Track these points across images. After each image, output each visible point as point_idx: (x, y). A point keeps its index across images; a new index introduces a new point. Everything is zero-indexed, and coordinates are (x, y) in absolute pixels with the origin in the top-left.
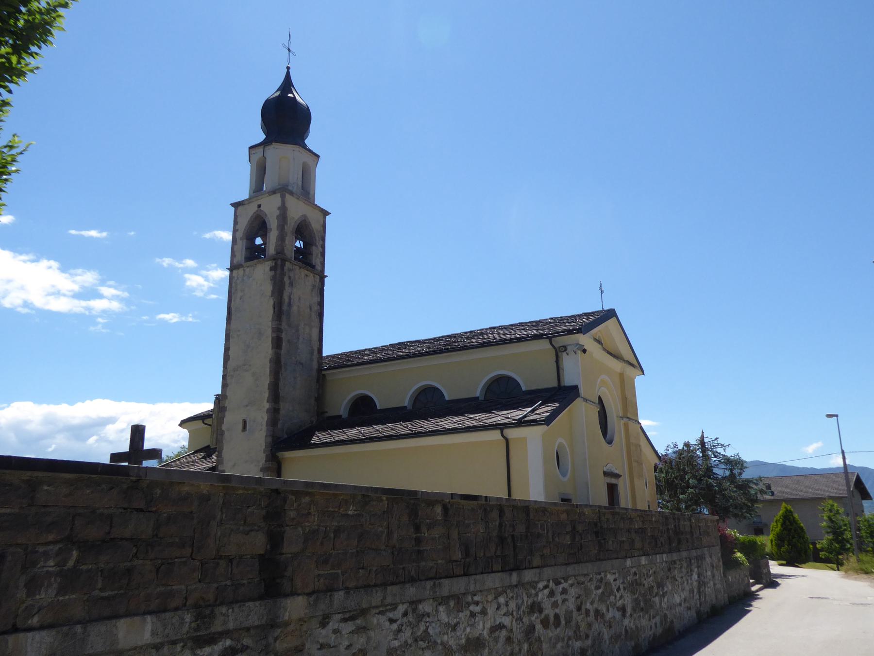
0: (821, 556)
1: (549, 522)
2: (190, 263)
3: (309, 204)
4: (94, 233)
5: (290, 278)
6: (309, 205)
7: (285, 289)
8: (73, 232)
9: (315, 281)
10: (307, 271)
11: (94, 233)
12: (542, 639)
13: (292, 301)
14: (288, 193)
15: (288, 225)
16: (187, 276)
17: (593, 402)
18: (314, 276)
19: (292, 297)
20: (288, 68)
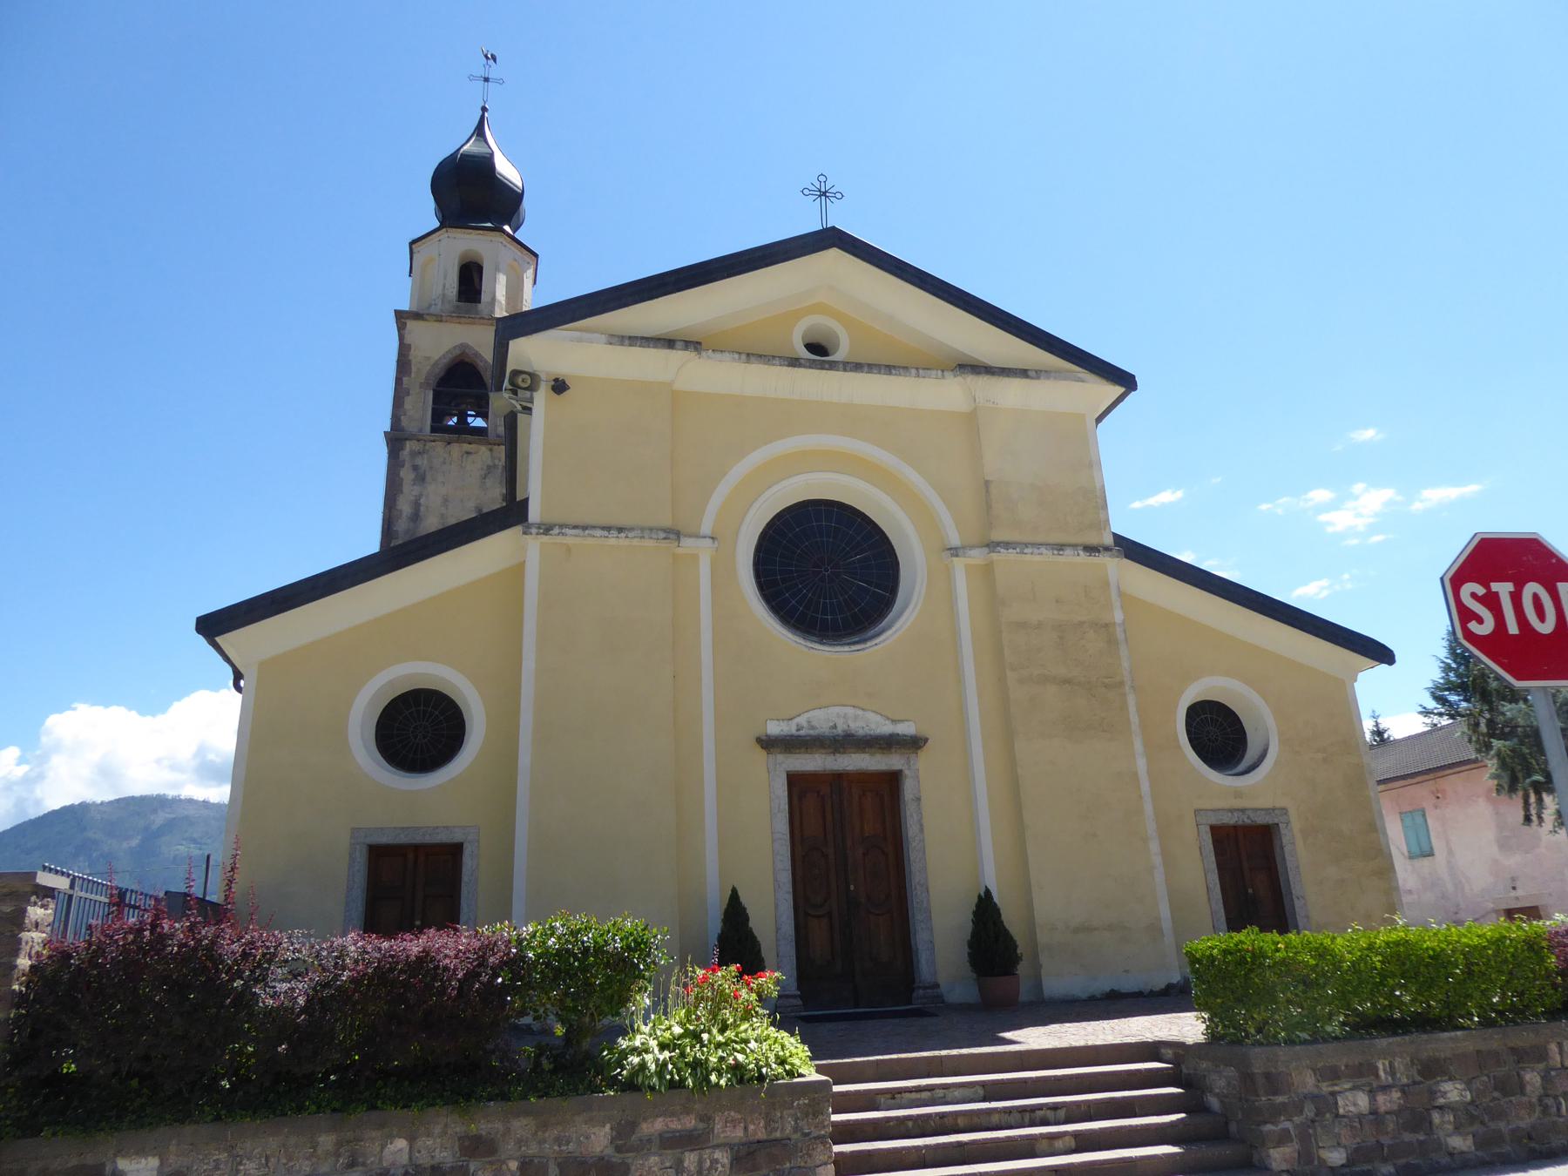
0: (524, 929)
1: (652, 943)
2: (1321, 495)
3: (482, 321)
4: (1166, 497)
5: (415, 468)
6: (474, 324)
7: (402, 492)
8: (1137, 505)
9: (493, 458)
10: (470, 444)
11: (1166, 497)
12: (42, 1134)
13: (422, 509)
14: (408, 318)
15: (413, 375)
16: (1323, 518)
17: (603, 528)
18: (491, 450)
19: (422, 501)
20: (484, 109)
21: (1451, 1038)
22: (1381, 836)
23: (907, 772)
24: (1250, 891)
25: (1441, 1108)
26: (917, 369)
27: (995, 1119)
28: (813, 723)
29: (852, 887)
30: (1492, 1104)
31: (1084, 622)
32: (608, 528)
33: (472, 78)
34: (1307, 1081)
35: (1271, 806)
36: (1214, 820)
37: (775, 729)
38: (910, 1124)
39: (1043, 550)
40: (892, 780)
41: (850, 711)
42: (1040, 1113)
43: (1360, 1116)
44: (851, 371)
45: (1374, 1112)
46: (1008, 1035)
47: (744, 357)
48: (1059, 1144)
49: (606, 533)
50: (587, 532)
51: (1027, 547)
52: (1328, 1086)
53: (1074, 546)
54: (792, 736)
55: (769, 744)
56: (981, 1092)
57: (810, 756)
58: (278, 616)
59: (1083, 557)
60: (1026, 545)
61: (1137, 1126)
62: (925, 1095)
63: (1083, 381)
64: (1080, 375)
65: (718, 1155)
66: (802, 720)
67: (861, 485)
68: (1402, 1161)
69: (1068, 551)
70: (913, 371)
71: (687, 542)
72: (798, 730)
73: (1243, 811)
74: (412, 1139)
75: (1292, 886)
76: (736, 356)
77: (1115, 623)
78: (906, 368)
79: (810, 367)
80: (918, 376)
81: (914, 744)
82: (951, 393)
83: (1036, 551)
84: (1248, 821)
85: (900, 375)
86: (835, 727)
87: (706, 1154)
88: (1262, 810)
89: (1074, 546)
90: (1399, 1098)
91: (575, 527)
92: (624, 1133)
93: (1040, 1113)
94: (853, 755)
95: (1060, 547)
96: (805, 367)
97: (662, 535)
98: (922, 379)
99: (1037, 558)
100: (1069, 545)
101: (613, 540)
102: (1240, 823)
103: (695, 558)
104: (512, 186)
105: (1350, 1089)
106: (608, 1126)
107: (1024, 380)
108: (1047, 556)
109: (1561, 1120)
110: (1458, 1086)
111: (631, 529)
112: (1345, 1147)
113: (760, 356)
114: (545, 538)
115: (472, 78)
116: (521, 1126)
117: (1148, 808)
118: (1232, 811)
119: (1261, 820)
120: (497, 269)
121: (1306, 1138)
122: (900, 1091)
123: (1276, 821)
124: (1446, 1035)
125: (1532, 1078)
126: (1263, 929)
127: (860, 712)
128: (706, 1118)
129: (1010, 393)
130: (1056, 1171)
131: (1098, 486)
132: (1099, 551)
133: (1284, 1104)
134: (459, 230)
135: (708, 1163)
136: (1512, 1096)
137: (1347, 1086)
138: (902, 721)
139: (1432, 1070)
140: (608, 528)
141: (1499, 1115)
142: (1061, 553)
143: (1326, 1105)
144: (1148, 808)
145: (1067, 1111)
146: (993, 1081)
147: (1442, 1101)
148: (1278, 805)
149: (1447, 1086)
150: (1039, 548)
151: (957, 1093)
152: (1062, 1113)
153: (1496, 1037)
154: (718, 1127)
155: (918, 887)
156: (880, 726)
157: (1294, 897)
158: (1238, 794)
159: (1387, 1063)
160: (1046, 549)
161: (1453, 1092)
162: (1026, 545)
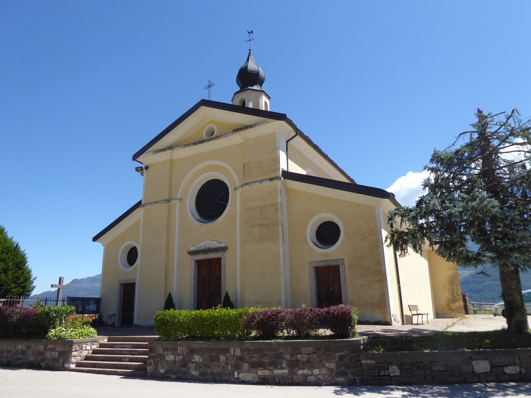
20: (250, 50)
21: (199, 343)
22: (382, 267)
23: (222, 258)
24: (331, 289)
25: (192, 362)
26: (225, 135)
27: (125, 352)
28: (201, 246)
29: (212, 291)
30: (207, 363)
31: (268, 204)
32: (154, 203)
33: (246, 42)
34: (161, 351)
35: (338, 258)
36: (315, 265)
37: (192, 249)
38: (110, 352)
39: (257, 183)
40: (219, 260)
41: (209, 241)
42: (133, 352)
43: (171, 361)
44: (208, 141)
45: (175, 361)
46: (428, 333)
47: (184, 146)
48: (126, 360)
49: (154, 204)
50: (151, 204)
51: (252, 183)
52: (166, 352)
53: (266, 180)
54: (196, 250)
55: (191, 253)
56: (132, 346)
57: (200, 255)
58: (103, 236)
59: (269, 183)
60: (252, 183)
61: (140, 357)
62: (122, 346)
63: (269, 123)
64: (268, 121)
65: (57, 353)
66: (198, 246)
67: (202, 177)
68: (178, 375)
69: (264, 182)
70: (224, 136)
71: (173, 202)
72: (197, 248)
73: (326, 261)
74: (22, 345)
75: (342, 287)
76: (182, 147)
77: (278, 203)
78: (222, 135)
79: (199, 144)
80: (225, 137)
81: (224, 249)
82: (237, 138)
83: (255, 184)
84: (328, 265)
85: (221, 138)
86: (206, 247)
87: (55, 352)
88: (333, 260)
89: (266, 180)
90: (181, 358)
91: (149, 204)
92: (45, 347)
93: (133, 352)
94: (210, 254)
95: (262, 181)
96: (197, 144)
97: (165, 202)
98: (227, 137)
99: (256, 186)
100: (264, 180)
101: (156, 205)
102: (325, 265)
103: (176, 205)
104: (255, 72)
105: (171, 354)
106: (43, 346)
107: (252, 128)
108: (258, 185)
109: (228, 372)
110: (199, 357)
111: (158, 202)
112: (165, 369)
113: (187, 145)
114: (144, 208)
115: (246, 42)
116: (33, 344)
117: (282, 263)
118: (322, 261)
119: (332, 264)
120: (249, 101)
121: (156, 364)
122: (117, 344)
123: (338, 264)
124: (197, 342)
125: (222, 358)
126: (204, 309)
127: (212, 241)
128: (56, 346)
129: (250, 133)
130: (114, 365)
131: (278, 156)
132: (274, 179)
133: (153, 356)
134: (238, 94)
135: (55, 355)
136: (214, 362)
137: (170, 353)
138: (222, 243)
139: (192, 351)
140: (154, 203)
141: (209, 367)
142: (262, 183)
143: (162, 357)
144: (282, 263)
145: (138, 353)
146: (142, 344)
147: (193, 360)
148: (340, 258)
149: (195, 357)
150: (255, 183)
151: (127, 346)
152: (137, 353)
153: (212, 344)
154: (57, 348)
155: (223, 290)
156: (216, 245)
157: (342, 291)
158: (326, 255)
159: (181, 348)
160: (258, 183)
161: (197, 358)
162: (252, 183)
